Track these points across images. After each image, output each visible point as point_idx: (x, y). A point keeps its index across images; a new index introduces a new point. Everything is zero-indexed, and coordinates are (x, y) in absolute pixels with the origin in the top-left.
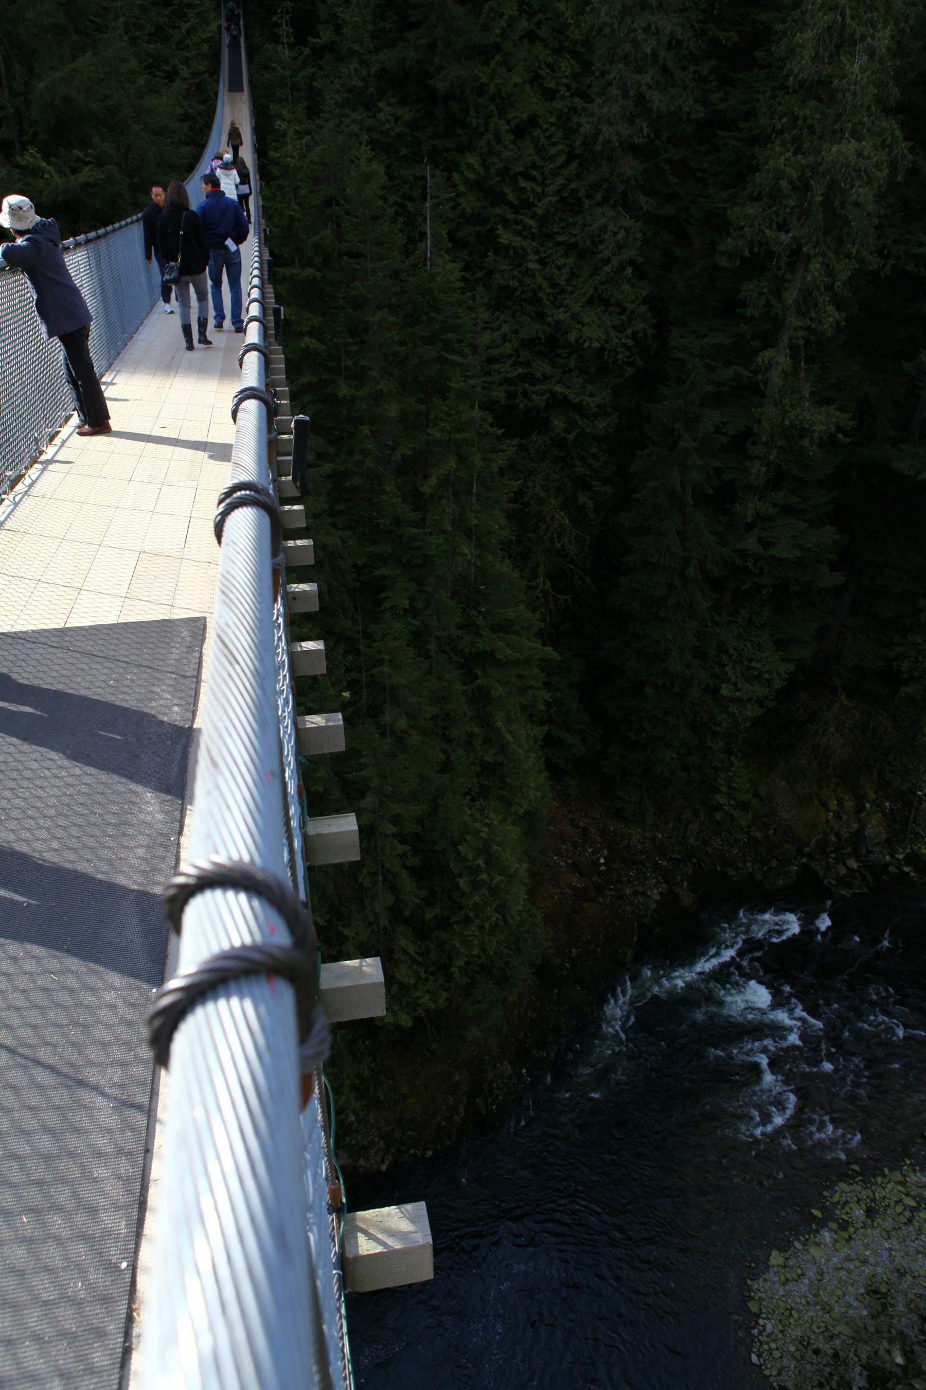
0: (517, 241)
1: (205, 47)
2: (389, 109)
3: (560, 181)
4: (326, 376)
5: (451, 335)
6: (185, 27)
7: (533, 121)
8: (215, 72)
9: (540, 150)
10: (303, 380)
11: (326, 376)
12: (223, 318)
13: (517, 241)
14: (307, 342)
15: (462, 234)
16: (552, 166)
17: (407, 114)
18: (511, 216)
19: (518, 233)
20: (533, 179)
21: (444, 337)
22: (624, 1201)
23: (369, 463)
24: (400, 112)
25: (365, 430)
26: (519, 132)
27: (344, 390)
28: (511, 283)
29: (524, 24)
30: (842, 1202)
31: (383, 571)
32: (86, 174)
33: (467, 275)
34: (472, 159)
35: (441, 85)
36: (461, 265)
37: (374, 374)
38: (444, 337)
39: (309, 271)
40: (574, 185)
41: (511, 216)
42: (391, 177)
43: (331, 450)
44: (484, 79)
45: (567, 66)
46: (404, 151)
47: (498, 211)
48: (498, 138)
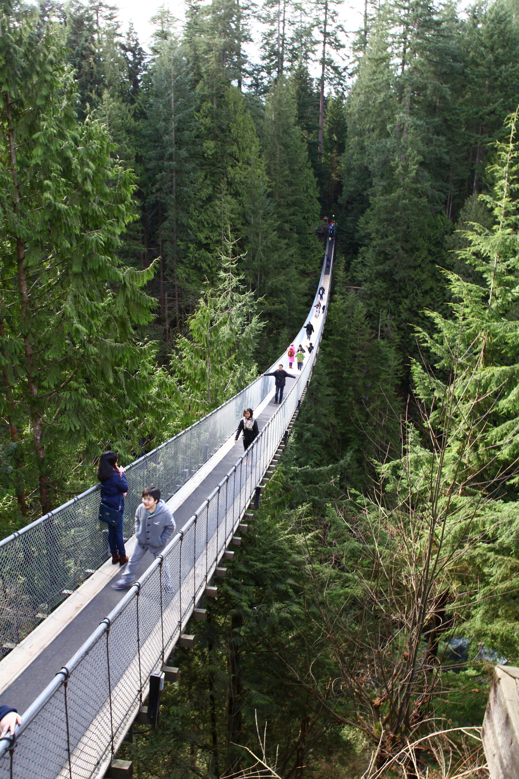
1: (319, 261)
7: (432, 289)
8: (320, 268)
9: (433, 299)
12: (264, 563)
15: (402, 326)
17: (384, 285)
23: (350, 399)
24: (382, 284)
25: (351, 388)
26: (426, 293)
27: (345, 375)
29: (430, 258)
30: (123, 52)
31: (350, 435)
32: (276, 307)
34: (407, 301)
39: (339, 338)
41: (420, 321)
42: (377, 305)
44: (413, 276)
46: (383, 297)
47: (416, 319)
48: (416, 295)
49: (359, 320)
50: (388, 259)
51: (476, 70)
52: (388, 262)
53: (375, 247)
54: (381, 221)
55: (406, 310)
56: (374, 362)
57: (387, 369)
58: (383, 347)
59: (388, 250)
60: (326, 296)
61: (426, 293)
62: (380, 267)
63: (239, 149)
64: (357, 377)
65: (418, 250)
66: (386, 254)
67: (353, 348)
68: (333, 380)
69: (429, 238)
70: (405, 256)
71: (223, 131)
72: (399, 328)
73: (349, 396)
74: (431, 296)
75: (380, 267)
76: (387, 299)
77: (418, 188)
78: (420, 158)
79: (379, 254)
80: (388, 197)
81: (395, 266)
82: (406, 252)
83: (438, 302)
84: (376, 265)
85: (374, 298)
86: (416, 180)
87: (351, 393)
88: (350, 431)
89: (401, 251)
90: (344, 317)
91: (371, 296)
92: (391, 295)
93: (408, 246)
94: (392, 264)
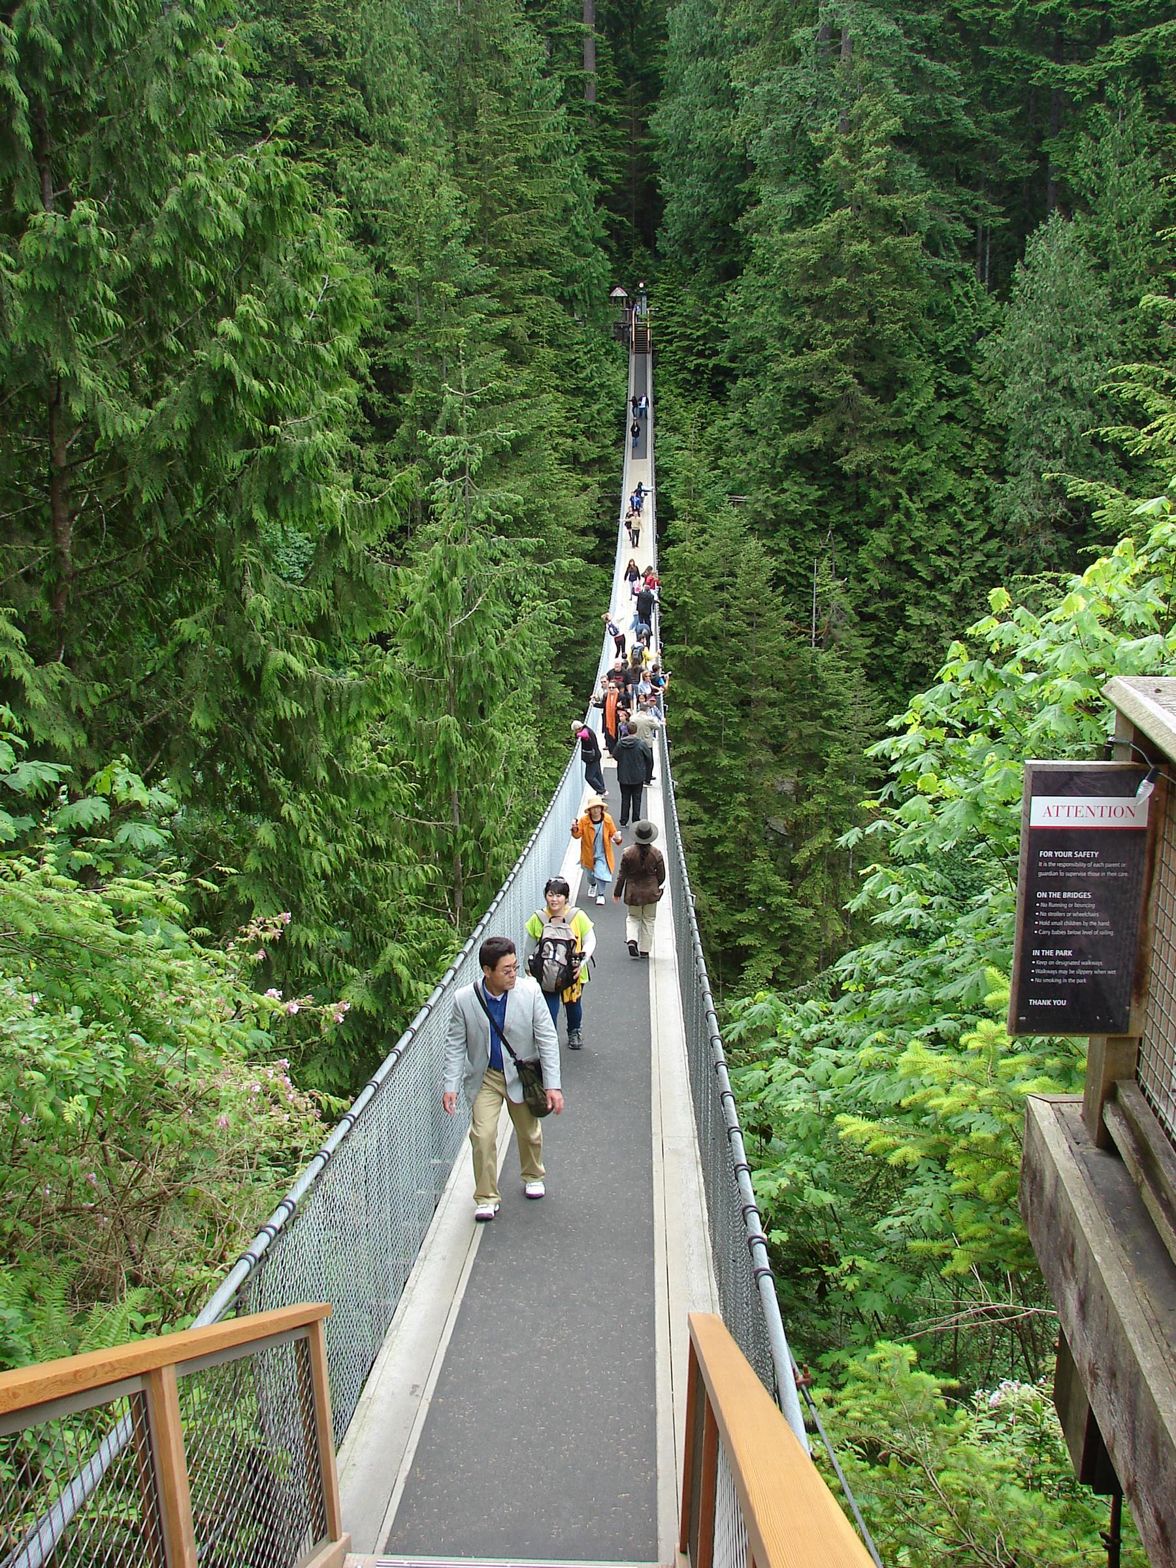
0: (930, 618)
2: (796, 488)
3: (979, 557)
4: (706, 747)
5: (832, 712)
6: (596, 407)
8: (619, 441)
9: (958, 525)
10: (685, 749)
11: (706, 747)
13: (930, 618)
14: (692, 714)
15: (870, 610)
16: (969, 542)
17: (814, 493)
18: (923, 592)
19: (933, 609)
20: (949, 554)
21: (824, 714)
22: (502, 519)
24: (806, 490)
25: (741, 797)
28: (925, 661)
29: (943, 408)
33: (876, 651)
35: (848, 466)
36: (869, 641)
37: (752, 744)
38: (824, 714)
40: (991, 564)
41: (923, 592)
43: (706, 817)
45: (983, 448)
49: (754, 595)
50: (818, 412)
51: (953, 1427)
52: (819, 422)
53: (780, 379)
54: (789, 304)
55: (879, 562)
56: (804, 717)
57: (843, 735)
58: (826, 668)
59: (817, 386)
60: (647, 523)
61: (934, 507)
62: (795, 439)
63: (367, 104)
64: (759, 764)
65: (905, 384)
66: (813, 399)
67: (740, 680)
68: (688, 777)
69: (934, 348)
70: (868, 400)
71: (319, 53)
72: (865, 618)
73: (738, 819)
74: (951, 517)
75: (795, 439)
76: (822, 528)
77: (895, 209)
78: (893, 124)
79: (793, 397)
80: (808, 233)
81: (841, 429)
82: (872, 390)
83: (971, 533)
84: (787, 432)
85: (786, 529)
86: (885, 186)
87: (744, 813)
88: (747, 928)
89: (856, 389)
90: (708, 585)
91: (775, 526)
92: (834, 520)
93: (876, 373)
94: (831, 427)
